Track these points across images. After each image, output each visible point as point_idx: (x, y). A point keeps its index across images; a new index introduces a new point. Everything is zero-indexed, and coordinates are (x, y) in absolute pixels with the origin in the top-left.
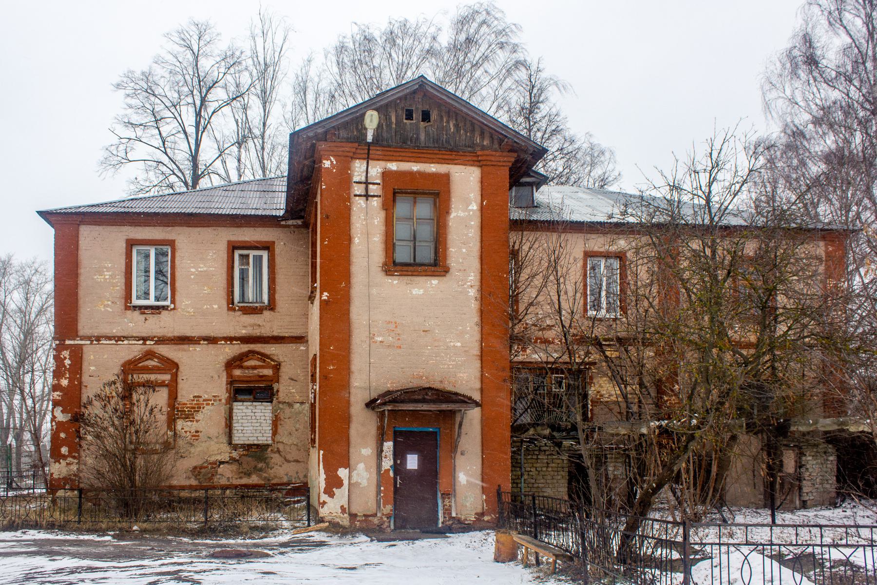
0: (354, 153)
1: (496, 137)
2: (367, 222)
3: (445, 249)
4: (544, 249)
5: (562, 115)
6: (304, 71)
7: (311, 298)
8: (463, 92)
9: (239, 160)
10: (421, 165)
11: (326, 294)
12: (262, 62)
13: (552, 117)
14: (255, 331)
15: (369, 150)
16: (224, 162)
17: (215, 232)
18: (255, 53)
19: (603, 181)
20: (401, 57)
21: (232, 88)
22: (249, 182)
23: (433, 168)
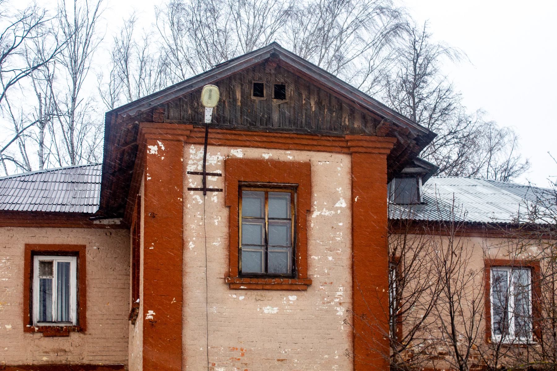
0: (188, 137)
1: (369, 118)
2: (204, 224)
3: (306, 257)
4: (432, 260)
5: (456, 90)
6: (125, 34)
7: (133, 316)
8: (329, 63)
9: (41, 144)
10: (274, 151)
11: (151, 312)
12: (72, 22)
13: (442, 93)
14: (59, 358)
15: (207, 133)
16: (23, 145)
17: (8, 233)
18: (63, 13)
19: (507, 172)
20: (252, 18)
21: (32, 56)
22: (53, 171)
23: (289, 156)
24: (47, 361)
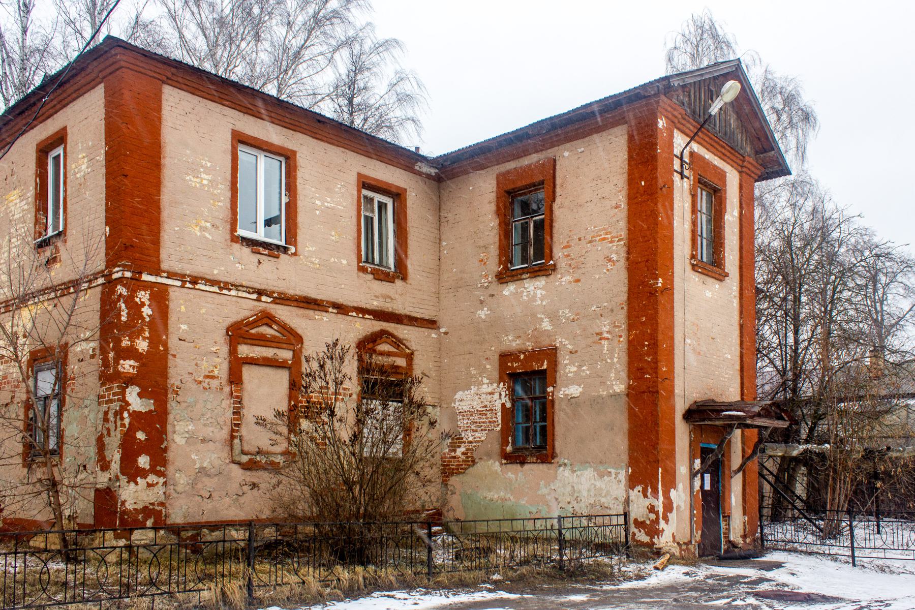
24: (730, 504)
